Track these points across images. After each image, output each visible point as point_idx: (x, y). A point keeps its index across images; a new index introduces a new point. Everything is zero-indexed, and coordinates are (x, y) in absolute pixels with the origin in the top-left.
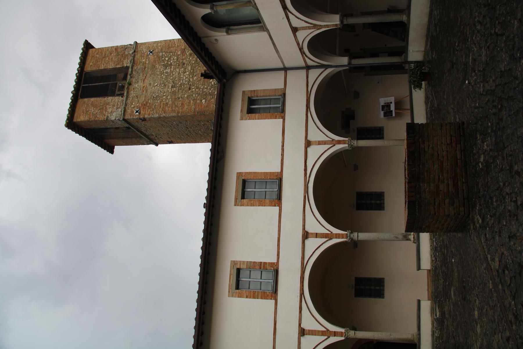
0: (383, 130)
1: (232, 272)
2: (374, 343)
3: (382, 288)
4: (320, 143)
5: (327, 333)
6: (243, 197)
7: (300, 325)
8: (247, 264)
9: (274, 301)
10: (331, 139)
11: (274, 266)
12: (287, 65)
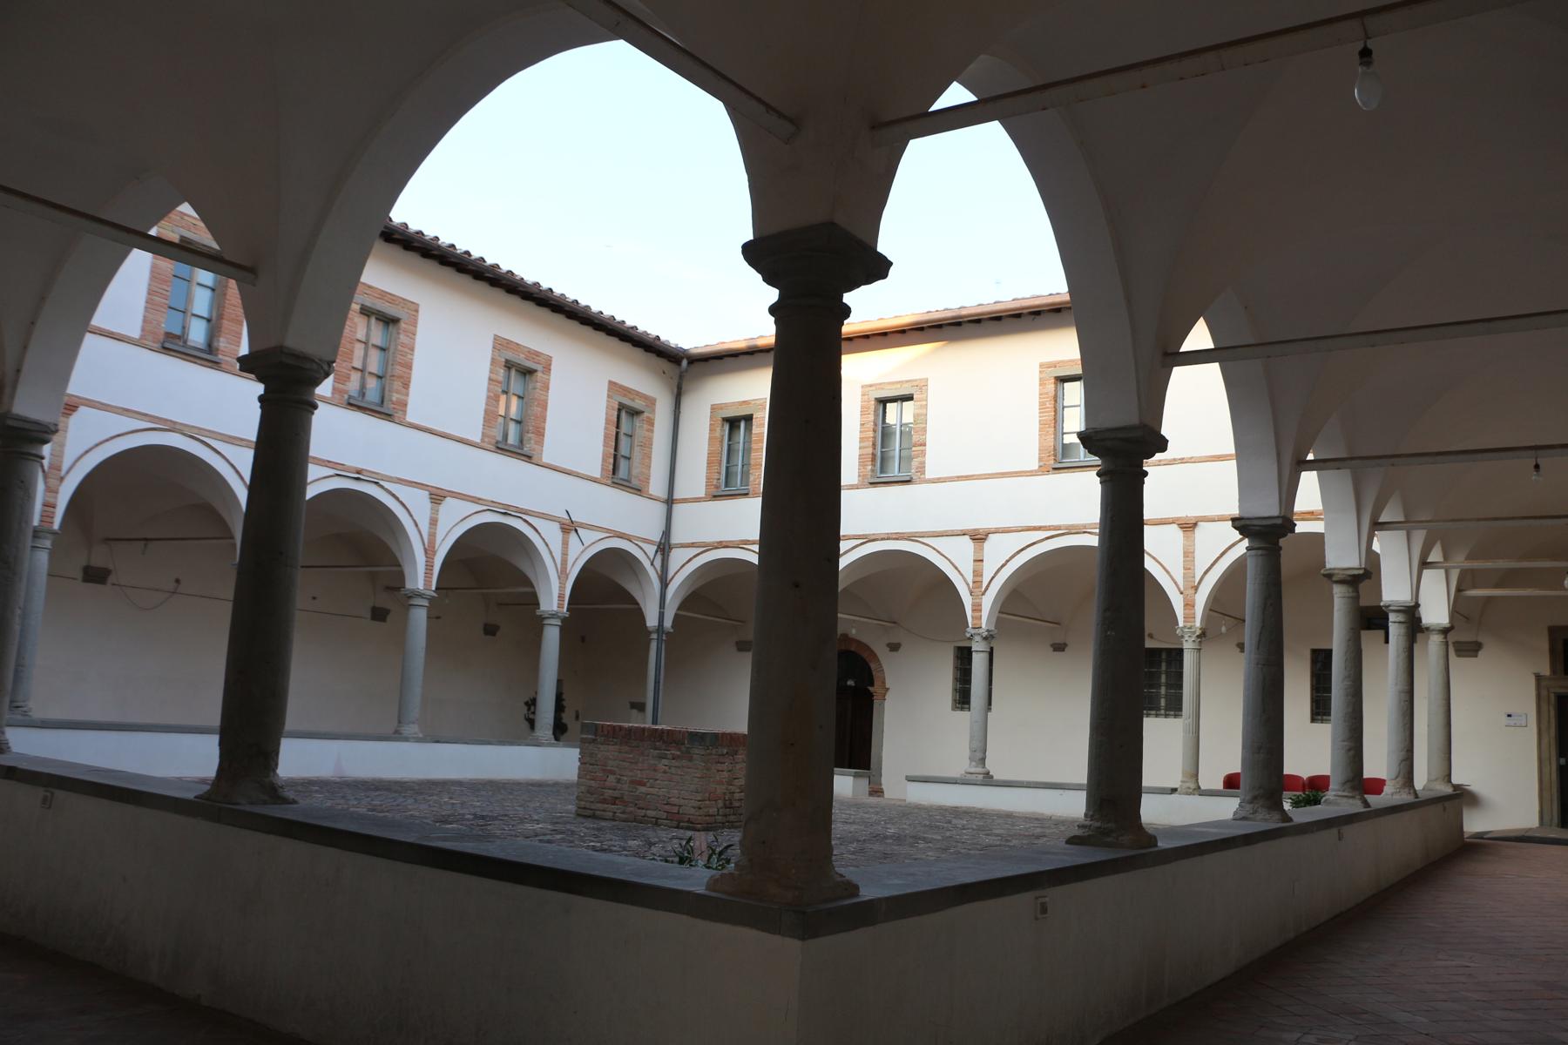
0: (954, 701)
1: (906, 385)
2: (870, 688)
3: (1163, 712)
4: (1189, 555)
5: (977, 588)
6: (509, 365)
7: (997, 531)
9: (856, 483)
10: (1200, 583)
12: (677, 508)
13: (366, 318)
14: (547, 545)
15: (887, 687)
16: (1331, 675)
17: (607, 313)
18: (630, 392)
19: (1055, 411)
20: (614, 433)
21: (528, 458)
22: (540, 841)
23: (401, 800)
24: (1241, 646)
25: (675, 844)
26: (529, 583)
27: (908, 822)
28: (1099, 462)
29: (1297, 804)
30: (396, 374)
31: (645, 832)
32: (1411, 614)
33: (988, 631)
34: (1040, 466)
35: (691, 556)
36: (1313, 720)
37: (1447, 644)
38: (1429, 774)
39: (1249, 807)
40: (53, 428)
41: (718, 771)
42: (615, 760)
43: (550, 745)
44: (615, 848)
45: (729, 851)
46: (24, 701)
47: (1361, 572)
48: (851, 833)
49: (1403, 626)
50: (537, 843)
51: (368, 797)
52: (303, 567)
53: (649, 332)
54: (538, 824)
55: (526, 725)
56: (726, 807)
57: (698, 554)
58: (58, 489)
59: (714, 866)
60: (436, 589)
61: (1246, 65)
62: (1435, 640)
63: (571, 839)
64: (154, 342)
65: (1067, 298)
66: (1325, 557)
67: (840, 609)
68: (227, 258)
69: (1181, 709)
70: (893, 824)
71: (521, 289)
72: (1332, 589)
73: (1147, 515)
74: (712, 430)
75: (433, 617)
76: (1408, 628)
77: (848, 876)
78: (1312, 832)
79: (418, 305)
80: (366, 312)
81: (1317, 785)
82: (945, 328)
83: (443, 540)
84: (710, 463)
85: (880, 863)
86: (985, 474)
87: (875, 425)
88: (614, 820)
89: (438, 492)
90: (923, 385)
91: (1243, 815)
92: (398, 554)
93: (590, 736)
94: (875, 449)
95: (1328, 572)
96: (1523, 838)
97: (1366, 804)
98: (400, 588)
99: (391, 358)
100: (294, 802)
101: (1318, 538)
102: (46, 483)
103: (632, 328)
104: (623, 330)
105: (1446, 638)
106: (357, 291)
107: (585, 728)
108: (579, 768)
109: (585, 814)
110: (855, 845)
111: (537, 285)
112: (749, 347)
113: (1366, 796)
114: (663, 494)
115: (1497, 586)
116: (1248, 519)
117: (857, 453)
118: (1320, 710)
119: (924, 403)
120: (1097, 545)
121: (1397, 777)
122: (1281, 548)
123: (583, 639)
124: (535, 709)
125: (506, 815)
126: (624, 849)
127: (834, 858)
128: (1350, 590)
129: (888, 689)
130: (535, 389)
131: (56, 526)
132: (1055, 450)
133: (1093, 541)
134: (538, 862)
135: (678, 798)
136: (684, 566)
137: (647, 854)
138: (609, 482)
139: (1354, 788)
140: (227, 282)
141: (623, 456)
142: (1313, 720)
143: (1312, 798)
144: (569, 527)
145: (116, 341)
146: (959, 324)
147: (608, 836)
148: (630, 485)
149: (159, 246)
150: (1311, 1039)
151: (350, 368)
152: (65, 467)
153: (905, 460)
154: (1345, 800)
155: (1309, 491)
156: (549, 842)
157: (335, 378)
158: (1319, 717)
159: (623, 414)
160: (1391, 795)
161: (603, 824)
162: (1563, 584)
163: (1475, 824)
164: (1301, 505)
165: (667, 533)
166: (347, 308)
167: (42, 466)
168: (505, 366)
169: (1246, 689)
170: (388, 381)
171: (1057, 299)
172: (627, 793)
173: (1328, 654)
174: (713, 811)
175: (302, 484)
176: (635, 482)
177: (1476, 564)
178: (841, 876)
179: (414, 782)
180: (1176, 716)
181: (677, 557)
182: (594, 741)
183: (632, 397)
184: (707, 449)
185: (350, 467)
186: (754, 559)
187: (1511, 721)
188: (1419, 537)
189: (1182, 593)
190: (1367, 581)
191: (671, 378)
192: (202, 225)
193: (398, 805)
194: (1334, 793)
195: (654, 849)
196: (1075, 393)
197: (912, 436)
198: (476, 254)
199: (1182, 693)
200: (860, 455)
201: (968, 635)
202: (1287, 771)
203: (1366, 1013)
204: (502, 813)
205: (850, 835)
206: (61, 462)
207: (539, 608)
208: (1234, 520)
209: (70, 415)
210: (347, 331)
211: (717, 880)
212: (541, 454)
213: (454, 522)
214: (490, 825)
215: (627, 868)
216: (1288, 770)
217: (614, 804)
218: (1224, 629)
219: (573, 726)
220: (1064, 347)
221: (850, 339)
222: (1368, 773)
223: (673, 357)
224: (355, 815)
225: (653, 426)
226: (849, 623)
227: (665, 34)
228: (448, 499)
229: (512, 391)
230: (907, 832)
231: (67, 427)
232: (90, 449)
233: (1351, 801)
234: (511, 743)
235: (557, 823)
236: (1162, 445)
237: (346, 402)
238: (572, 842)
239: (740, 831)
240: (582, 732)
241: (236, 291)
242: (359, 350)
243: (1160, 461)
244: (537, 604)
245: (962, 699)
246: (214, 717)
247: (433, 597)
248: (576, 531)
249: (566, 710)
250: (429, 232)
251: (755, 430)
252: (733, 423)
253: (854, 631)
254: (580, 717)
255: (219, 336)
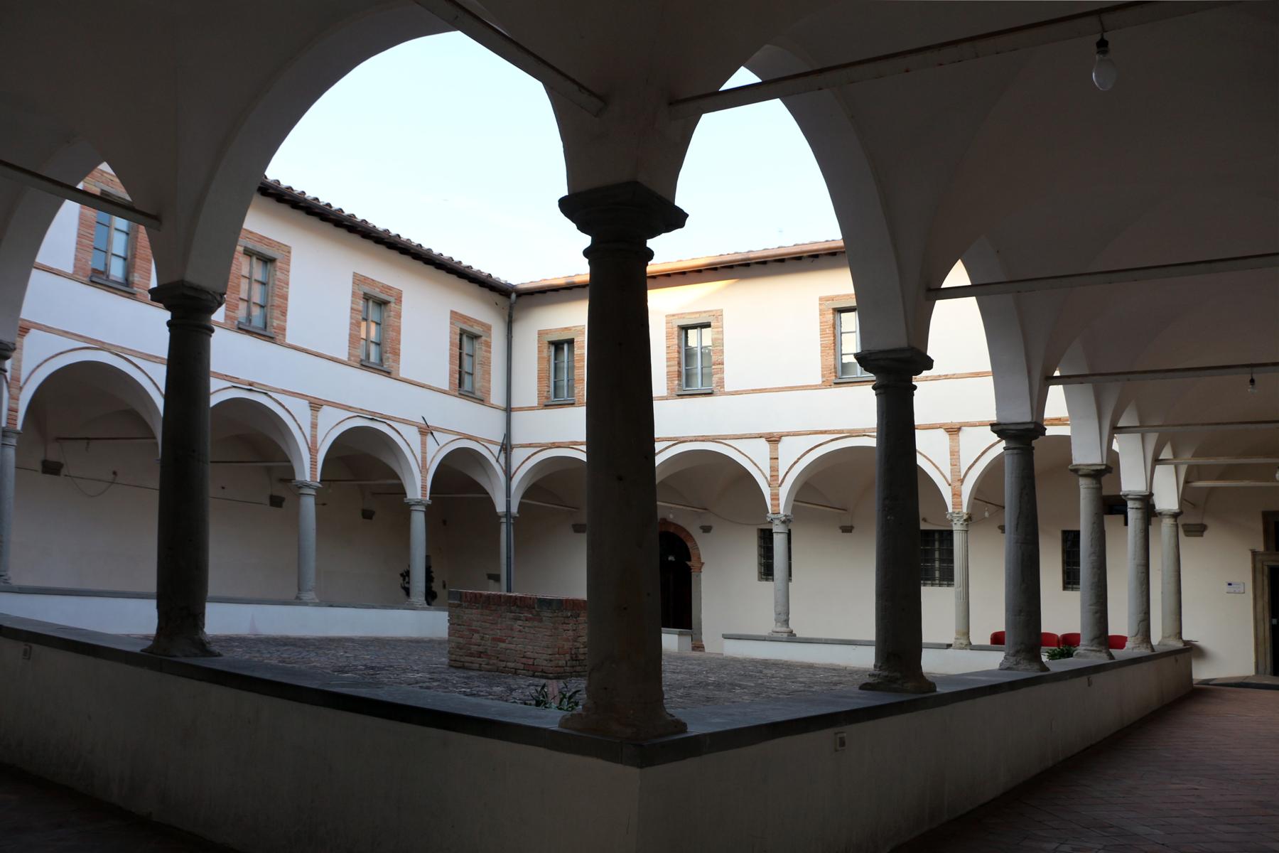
0: (760, 573)
1: (704, 315)
2: (688, 563)
3: (937, 582)
4: (955, 454)
5: (774, 481)
6: (367, 297)
7: (788, 435)
8: (719, 339)
9: (666, 395)
10: (965, 476)
11: (719, 387)
12: (514, 415)
13: (248, 258)
14: (409, 445)
15: (702, 561)
16: (1079, 551)
17: (446, 254)
18: (468, 320)
19: (834, 336)
20: (458, 354)
21: (388, 373)
22: (421, 687)
23: (305, 654)
24: (1002, 528)
25: (532, 690)
26: (396, 476)
27: (726, 672)
28: (874, 378)
29: (1053, 656)
30: (275, 304)
31: (507, 680)
32: (1146, 502)
33: (785, 516)
34: (823, 382)
35: (530, 454)
36: (1065, 588)
37: (1177, 526)
38: (1163, 632)
39: (1012, 659)
40: (11, 346)
41: (565, 630)
42: (478, 621)
43: (423, 609)
44: (482, 693)
45: (577, 695)
46: (5, 571)
47: (1103, 467)
48: (678, 680)
49: (1140, 511)
50: (418, 689)
51: (278, 651)
52: (211, 462)
53: (482, 271)
54: (418, 673)
55: (402, 592)
56: (572, 659)
57: (535, 453)
58: (18, 397)
59: (566, 708)
60: (321, 480)
61: (997, 53)
62: (1167, 523)
63: (446, 686)
64: (84, 277)
65: (842, 244)
66: (1071, 455)
67: (658, 497)
68: (137, 208)
69: (952, 580)
70: (714, 673)
71: (374, 235)
72: (1079, 482)
73: (917, 421)
74: (540, 351)
75: (320, 504)
76: (1144, 513)
77: (678, 716)
78: (1066, 679)
79: (290, 247)
80: (249, 253)
81: (1068, 643)
82: (735, 268)
83: (323, 440)
84: (540, 379)
85: (704, 705)
86: (776, 388)
87: (679, 347)
88: (480, 670)
89: (316, 401)
90: (719, 315)
91: (1008, 666)
92: (287, 453)
93: (456, 602)
94: (680, 367)
95: (1076, 467)
96: (1241, 684)
97: (1111, 657)
98: (291, 480)
99: (270, 291)
100: (220, 655)
101: (1065, 440)
102: (9, 392)
103: (468, 267)
104: (460, 269)
105: (1176, 521)
106: (241, 236)
107: (451, 595)
108: (449, 628)
109: (456, 665)
110: (682, 690)
111: (387, 231)
112: (568, 284)
113: (1110, 650)
114: (503, 404)
115: (1219, 478)
116: (1005, 424)
117: (665, 370)
118: (1070, 580)
119: (721, 329)
120: (875, 445)
121: (1137, 635)
122: (1033, 448)
123: (445, 522)
124: (409, 579)
125: (391, 666)
126: (490, 694)
127: (665, 701)
128: (1094, 482)
129: (703, 564)
130: (389, 316)
131: (19, 427)
132: (835, 368)
133: (872, 442)
134: (420, 704)
135: (532, 652)
136: (524, 461)
137: (510, 698)
138: (457, 394)
139: (1100, 644)
140: (138, 228)
141: (467, 373)
142: (1065, 588)
143: (1066, 652)
144: (426, 430)
145: (54, 275)
146: (748, 265)
147: (476, 683)
148: (474, 396)
149: (85, 198)
150: (1066, 848)
151: (238, 299)
152: (23, 379)
153: (706, 376)
154: (1093, 653)
155: (1056, 401)
156: (428, 688)
157: (226, 307)
158: (1070, 586)
159: (465, 339)
160: (1132, 649)
161: (471, 673)
162: (1275, 477)
163: (1201, 672)
164: (1048, 414)
165: (508, 435)
166: (234, 250)
167: (6, 378)
168: (364, 298)
169: (1008, 562)
170: (269, 310)
171: (833, 245)
172: (489, 648)
173: (1077, 533)
174: (562, 663)
175: (206, 394)
176: (478, 394)
177: (1201, 461)
178: (671, 715)
179: (314, 639)
180: (949, 585)
181: (518, 456)
182: (459, 606)
183: (471, 324)
184: (536, 366)
185: (242, 380)
186: (583, 457)
187: (1231, 589)
188: (1152, 439)
189: (950, 485)
190: (1108, 475)
191: (503, 308)
192: (117, 180)
193: (303, 658)
194: (1084, 648)
195: (514, 694)
196: (851, 322)
197: (711, 356)
198: (335, 206)
199: (953, 567)
200: (667, 372)
201: (769, 520)
202: (1044, 630)
203: (1112, 826)
204: (387, 664)
205: (677, 682)
206: (20, 374)
207: (406, 497)
208: (992, 425)
209: (24, 336)
210: (234, 268)
211: (567, 719)
212: (399, 370)
213: (331, 427)
214: (379, 674)
215: (493, 709)
216: (1045, 628)
217: (480, 657)
218: (987, 514)
219: (442, 594)
220: (840, 284)
221: (654, 277)
222: (1112, 631)
223: (503, 291)
224: (269, 665)
225: (490, 348)
226: (667, 509)
227: (495, 26)
228: (324, 407)
229: (370, 319)
230: (725, 680)
231: (22, 346)
232: (41, 364)
233: (1098, 654)
234: (392, 608)
235: (433, 673)
236: (928, 364)
237: (236, 328)
238: (447, 688)
239: (585, 680)
240: (449, 598)
241: (144, 231)
242: (244, 285)
243: (927, 377)
244: (404, 494)
245: (767, 571)
246: (152, 587)
247: (319, 487)
248: (432, 433)
249: (435, 580)
250: (298, 188)
251: (577, 351)
252: (558, 346)
253: (671, 516)
254: (447, 586)
255: (134, 272)
